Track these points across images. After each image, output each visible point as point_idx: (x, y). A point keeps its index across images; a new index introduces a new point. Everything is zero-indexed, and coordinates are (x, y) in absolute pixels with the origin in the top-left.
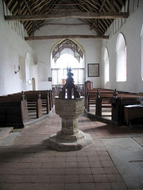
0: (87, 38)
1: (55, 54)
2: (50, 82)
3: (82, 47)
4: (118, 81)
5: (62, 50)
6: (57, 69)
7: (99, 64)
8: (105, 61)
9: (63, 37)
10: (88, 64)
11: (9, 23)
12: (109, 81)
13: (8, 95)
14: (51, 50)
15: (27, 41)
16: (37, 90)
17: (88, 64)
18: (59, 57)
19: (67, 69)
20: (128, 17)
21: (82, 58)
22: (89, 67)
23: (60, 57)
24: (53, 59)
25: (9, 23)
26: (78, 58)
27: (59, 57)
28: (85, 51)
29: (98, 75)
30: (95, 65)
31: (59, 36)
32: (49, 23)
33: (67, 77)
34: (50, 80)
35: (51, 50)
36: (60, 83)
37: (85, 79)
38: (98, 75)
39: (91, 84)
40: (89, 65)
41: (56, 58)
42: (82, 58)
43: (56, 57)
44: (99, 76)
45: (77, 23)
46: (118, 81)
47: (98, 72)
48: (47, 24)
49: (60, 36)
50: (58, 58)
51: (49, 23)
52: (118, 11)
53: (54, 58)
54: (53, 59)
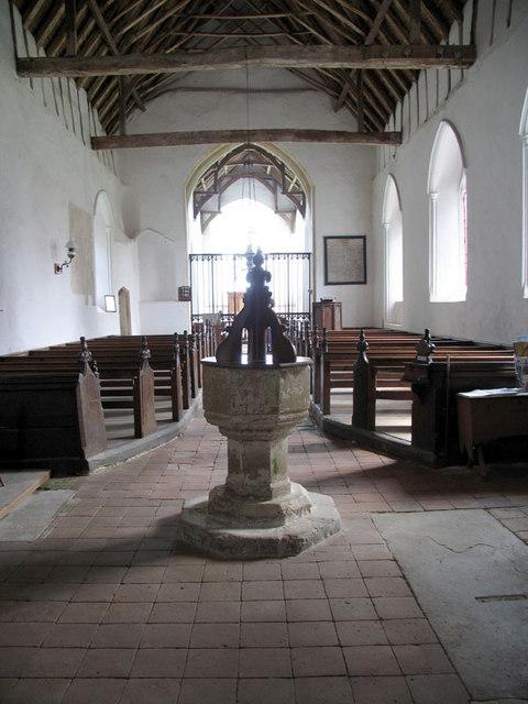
0: (320, 140)
1: (204, 200)
2: (185, 303)
3: (303, 176)
4: (434, 298)
5: (229, 184)
6: (210, 257)
7: (364, 238)
8: (387, 226)
9: (231, 137)
10: (326, 238)
11: (31, 86)
12: (401, 299)
13: (31, 353)
14: (189, 185)
15: (100, 151)
16: (135, 332)
17: (326, 238)
18: (219, 212)
19: (249, 256)
20: (471, 64)
21: (303, 214)
22: (328, 247)
23: (222, 209)
24: (195, 217)
25: (31, 86)
26: (289, 215)
27: (219, 212)
28: (314, 188)
29: (362, 280)
30: (351, 240)
31: (217, 132)
32: (180, 84)
33: (249, 285)
34: (185, 295)
35: (189, 185)
36: (220, 309)
37: (312, 292)
38: (362, 280)
39: (337, 310)
40: (328, 240)
41: (207, 216)
42: (303, 214)
43: (208, 212)
44: (365, 283)
45: (283, 86)
46: (434, 298)
47: (363, 268)
48: (175, 90)
49: (222, 132)
50: (214, 214)
51: (180, 84)
52: (435, 40)
53: (199, 216)
54: (195, 217)
